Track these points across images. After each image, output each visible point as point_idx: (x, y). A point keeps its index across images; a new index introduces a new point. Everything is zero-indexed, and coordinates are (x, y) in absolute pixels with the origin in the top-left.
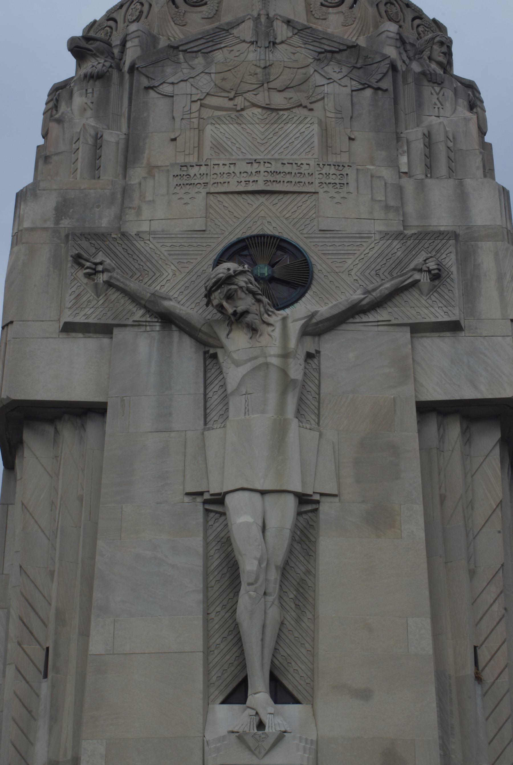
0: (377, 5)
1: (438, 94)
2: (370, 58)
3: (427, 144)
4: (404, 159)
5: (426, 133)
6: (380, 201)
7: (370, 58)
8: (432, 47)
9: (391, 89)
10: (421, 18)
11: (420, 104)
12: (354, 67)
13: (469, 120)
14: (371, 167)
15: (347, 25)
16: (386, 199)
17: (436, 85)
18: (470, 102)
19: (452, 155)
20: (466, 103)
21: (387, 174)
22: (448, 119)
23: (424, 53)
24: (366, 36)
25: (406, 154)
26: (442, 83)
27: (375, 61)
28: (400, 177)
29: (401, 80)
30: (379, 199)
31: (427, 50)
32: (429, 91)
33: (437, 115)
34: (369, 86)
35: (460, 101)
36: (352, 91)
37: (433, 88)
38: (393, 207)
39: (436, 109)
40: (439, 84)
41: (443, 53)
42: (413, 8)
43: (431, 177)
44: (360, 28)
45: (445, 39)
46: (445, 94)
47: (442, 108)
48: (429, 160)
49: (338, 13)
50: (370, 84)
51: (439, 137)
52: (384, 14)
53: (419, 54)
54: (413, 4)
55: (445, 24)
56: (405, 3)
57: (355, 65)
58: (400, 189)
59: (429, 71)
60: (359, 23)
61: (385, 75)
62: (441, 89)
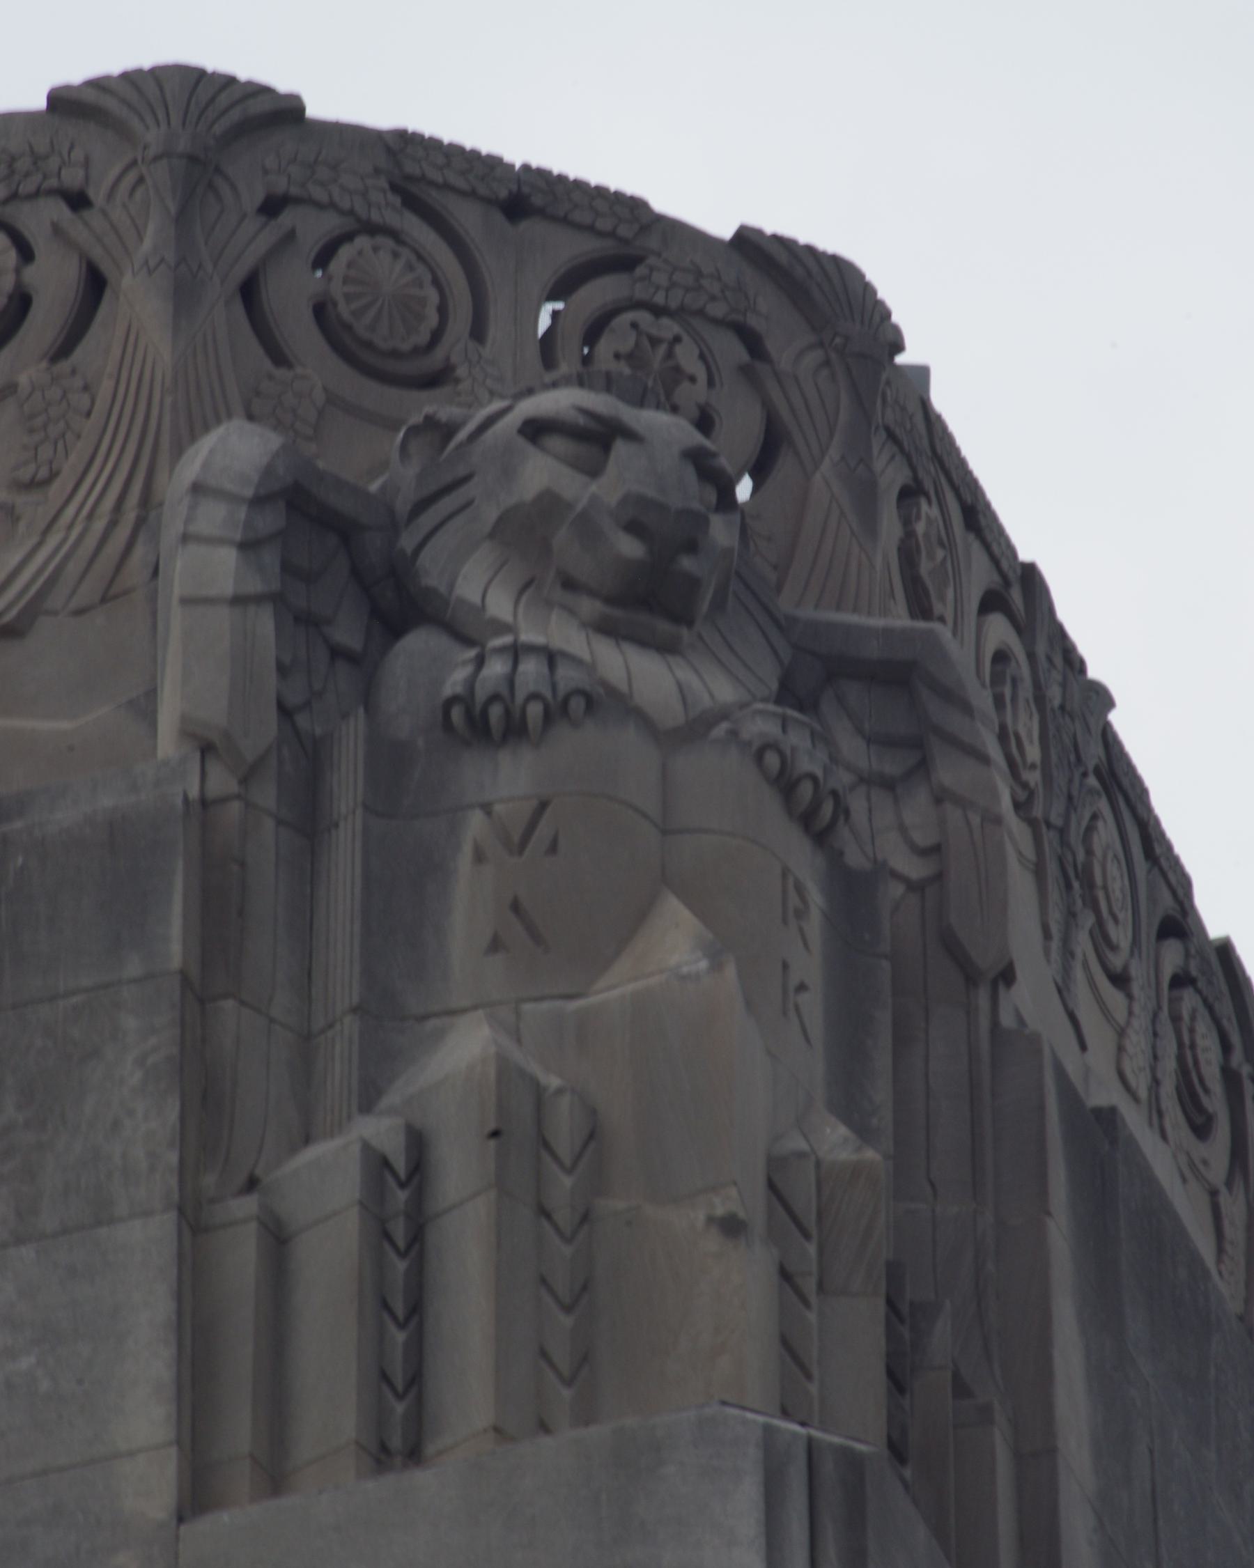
0: (249, 291)
10: (624, 263)
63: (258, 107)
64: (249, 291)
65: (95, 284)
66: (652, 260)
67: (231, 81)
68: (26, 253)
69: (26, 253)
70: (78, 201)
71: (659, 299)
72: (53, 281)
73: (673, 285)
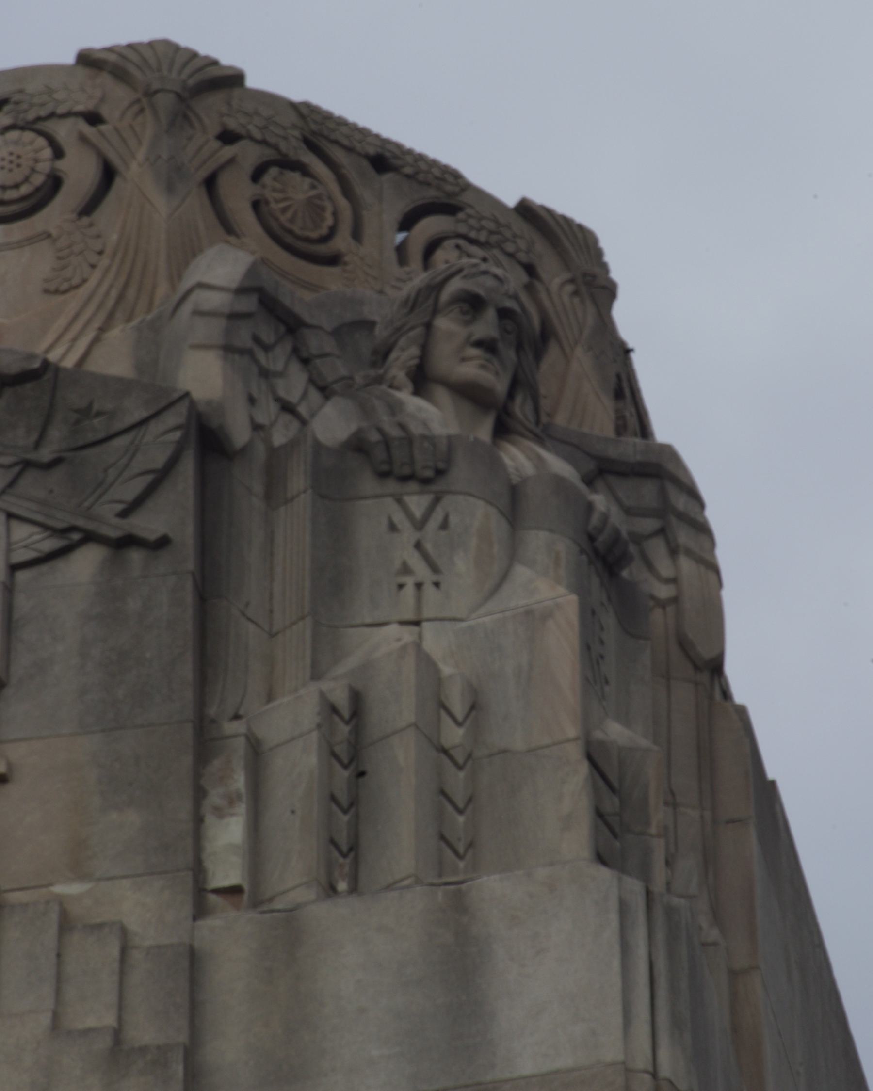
0: (210, 183)
1: (420, 525)
2: (99, 414)
3: (342, 750)
4: (228, 833)
5: (341, 698)
6: (87, 1032)
7: (99, 414)
8: (428, 326)
9: (186, 535)
10: (450, 209)
11: (332, 581)
12: (27, 464)
13: (547, 615)
14: (74, 889)
15: (65, 286)
16: (120, 1019)
17: (413, 486)
18: (591, 538)
19: (457, 782)
20: (564, 546)
21: (144, 908)
22: (464, 625)
23: (393, 355)
24: (134, 323)
25: (242, 808)
26: (440, 473)
27: (118, 426)
28: (200, 911)
29: (258, 487)
30: (91, 1022)
31: (402, 342)
32: (381, 520)
33: (410, 616)
34: (89, 537)
35: (537, 540)
36: (14, 568)
37: (399, 501)
38: (143, 1050)
39: (410, 590)
40: (426, 482)
41: (479, 344)
42: (408, 170)
43: (354, 889)
44: (114, 293)
45: (490, 282)
46: (453, 520)
47: (437, 585)
48: (346, 818)
49: (30, 240)
50: (91, 526)
51: (397, 708)
52: (246, 218)
53: (374, 365)
54: (410, 152)
55: (579, 217)
56: (367, 157)
57: (32, 456)
58: (193, 963)
59: (380, 430)
60: (114, 269)
61: (161, 477)
62: (437, 500)
63: (213, 72)
64: (210, 183)
65: (109, 174)
66: (469, 211)
67: (194, 55)
68: (58, 153)
69: (58, 153)
70: (93, 118)
71: (473, 234)
72: (79, 172)
73: (482, 228)
